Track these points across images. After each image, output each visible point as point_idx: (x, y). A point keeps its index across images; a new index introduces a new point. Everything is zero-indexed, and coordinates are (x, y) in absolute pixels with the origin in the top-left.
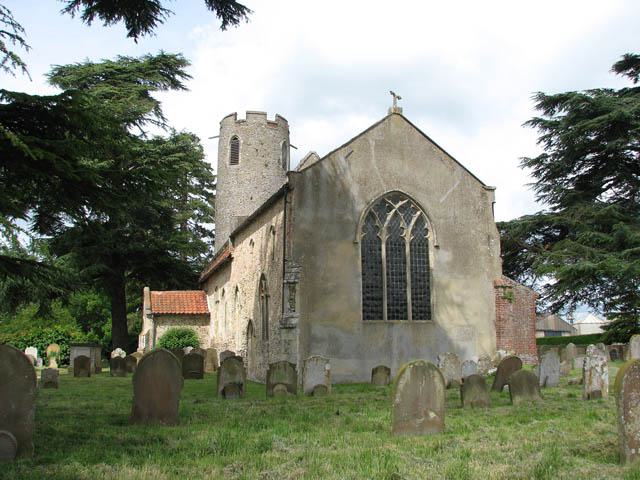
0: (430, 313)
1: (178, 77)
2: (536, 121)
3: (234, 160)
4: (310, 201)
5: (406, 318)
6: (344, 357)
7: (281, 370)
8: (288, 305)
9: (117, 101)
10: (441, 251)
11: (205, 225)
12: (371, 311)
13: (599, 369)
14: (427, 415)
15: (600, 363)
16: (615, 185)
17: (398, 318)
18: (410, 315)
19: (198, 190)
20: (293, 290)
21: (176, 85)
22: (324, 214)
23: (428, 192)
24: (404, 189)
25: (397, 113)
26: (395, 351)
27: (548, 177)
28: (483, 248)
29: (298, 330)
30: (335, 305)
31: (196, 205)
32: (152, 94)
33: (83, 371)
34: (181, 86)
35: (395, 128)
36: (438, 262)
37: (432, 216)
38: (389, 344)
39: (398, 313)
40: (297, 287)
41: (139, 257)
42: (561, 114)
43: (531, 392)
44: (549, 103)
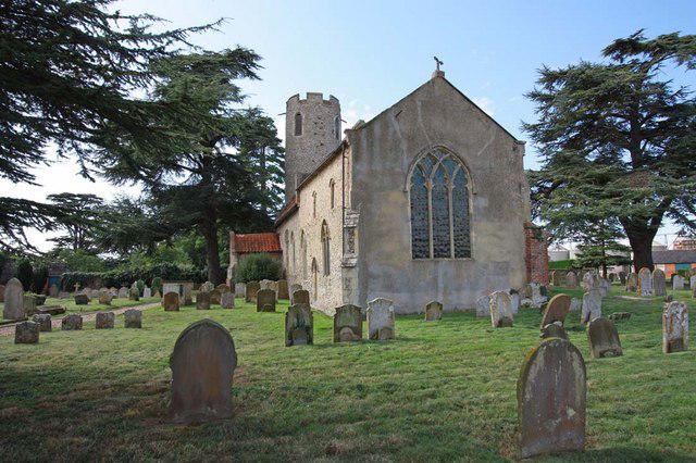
0: (469, 252)
1: (253, 70)
2: (534, 95)
3: (298, 132)
4: (365, 156)
5: (449, 257)
6: (398, 291)
7: (348, 314)
8: (348, 247)
9: (426, 386)
11: (279, 185)
12: (419, 252)
13: (679, 316)
14: (564, 413)
16: (600, 145)
19: (272, 159)
20: (352, 234)
21: (251, 75)
22: (378, 167)
23: (467, 146)
24: (447, 144)
25: (440, 75)
26: (441, 285)
28: (515, 195)
29: (358, 269)
30: (388, 246)
31: (272, 169)
32: (232, 81)
34: (256, 77)
35: (438, 90)
36: (476, 208)
37: (471, 167)
38: (435, 279)
39: (441, 253)
40: (356, 232)
41: (228, 207)
42: (558, 87)
44: (550, 77)
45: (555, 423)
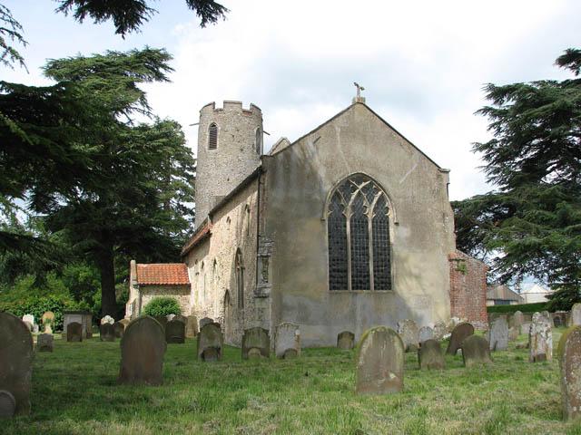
0: (390, 284)
1: (161, 70)
2: (486, 110)
3: (213, 145)
4: (281, 182)
5: (368, 289)
6: (312, 323)
7: (256, 336)
8: (261, 277)
9: (106, 92)
10: (400, 228)
11: (186, 204)
12: (337, 282)
13: (544, 335)
14: (387, 376)
15: (545, 329)
16: (558, 167)
17: (361, 288)
18: (372, 285)
19: (180, 172)
20: (266, 263)
21: (160, 77)
22: (294, 194)
23: (389, 174)
24: (367, 172)
25: (360, 102)
26: (359, 318)
28: (438, 225)
29: (271, 299)
30: (304, 277)
31: (178, 185)
32: (138, 85)
33: (75, 337)
34: (164, 78)
35: (359, 116)
36: (397, 238)
37: (392, 196)
38: (353, 312)
39: (361, 284)
40: (270, 261)
41: (126, 233)
42: (509, 103)
43: (482, 356)
44: (498, 93)
45: (380, 382)
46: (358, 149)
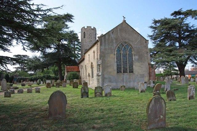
0: (133, 71)
1: (72, 20)
2: (151, 27)
3: (84, 37)
4: (103, 44)
5: (127, 73)
6: (113, 82)
7: (99, 89)
8: (98, 70)
11: (79, 52)
12: (119, 71)
13: (192, 89)
14: (160, 117)
15: (193, 88)
16: (170, 41)
19: (77, 45)
20: (100, 66)
21: (71, 21)
23: (132, 41)
24: (127, 41)
25: (125, 21)
26: (125, 81)
27: (154, 40)
28: (146, 55)
29: (101, 76)
30: (110, 70)
31: (77, 48)
32: (66, 23)
33: (49, 87)
36: (135, 59)
37: (133, 47)
38: (123, 79)
39: (125, 72)
40: (101, 66)
41: (65, 59)
42: (158, 25)
43: (173, 97)
44: (156, 22)
45: (157, 120)
46: (124, 35)
